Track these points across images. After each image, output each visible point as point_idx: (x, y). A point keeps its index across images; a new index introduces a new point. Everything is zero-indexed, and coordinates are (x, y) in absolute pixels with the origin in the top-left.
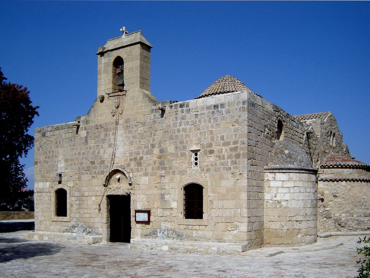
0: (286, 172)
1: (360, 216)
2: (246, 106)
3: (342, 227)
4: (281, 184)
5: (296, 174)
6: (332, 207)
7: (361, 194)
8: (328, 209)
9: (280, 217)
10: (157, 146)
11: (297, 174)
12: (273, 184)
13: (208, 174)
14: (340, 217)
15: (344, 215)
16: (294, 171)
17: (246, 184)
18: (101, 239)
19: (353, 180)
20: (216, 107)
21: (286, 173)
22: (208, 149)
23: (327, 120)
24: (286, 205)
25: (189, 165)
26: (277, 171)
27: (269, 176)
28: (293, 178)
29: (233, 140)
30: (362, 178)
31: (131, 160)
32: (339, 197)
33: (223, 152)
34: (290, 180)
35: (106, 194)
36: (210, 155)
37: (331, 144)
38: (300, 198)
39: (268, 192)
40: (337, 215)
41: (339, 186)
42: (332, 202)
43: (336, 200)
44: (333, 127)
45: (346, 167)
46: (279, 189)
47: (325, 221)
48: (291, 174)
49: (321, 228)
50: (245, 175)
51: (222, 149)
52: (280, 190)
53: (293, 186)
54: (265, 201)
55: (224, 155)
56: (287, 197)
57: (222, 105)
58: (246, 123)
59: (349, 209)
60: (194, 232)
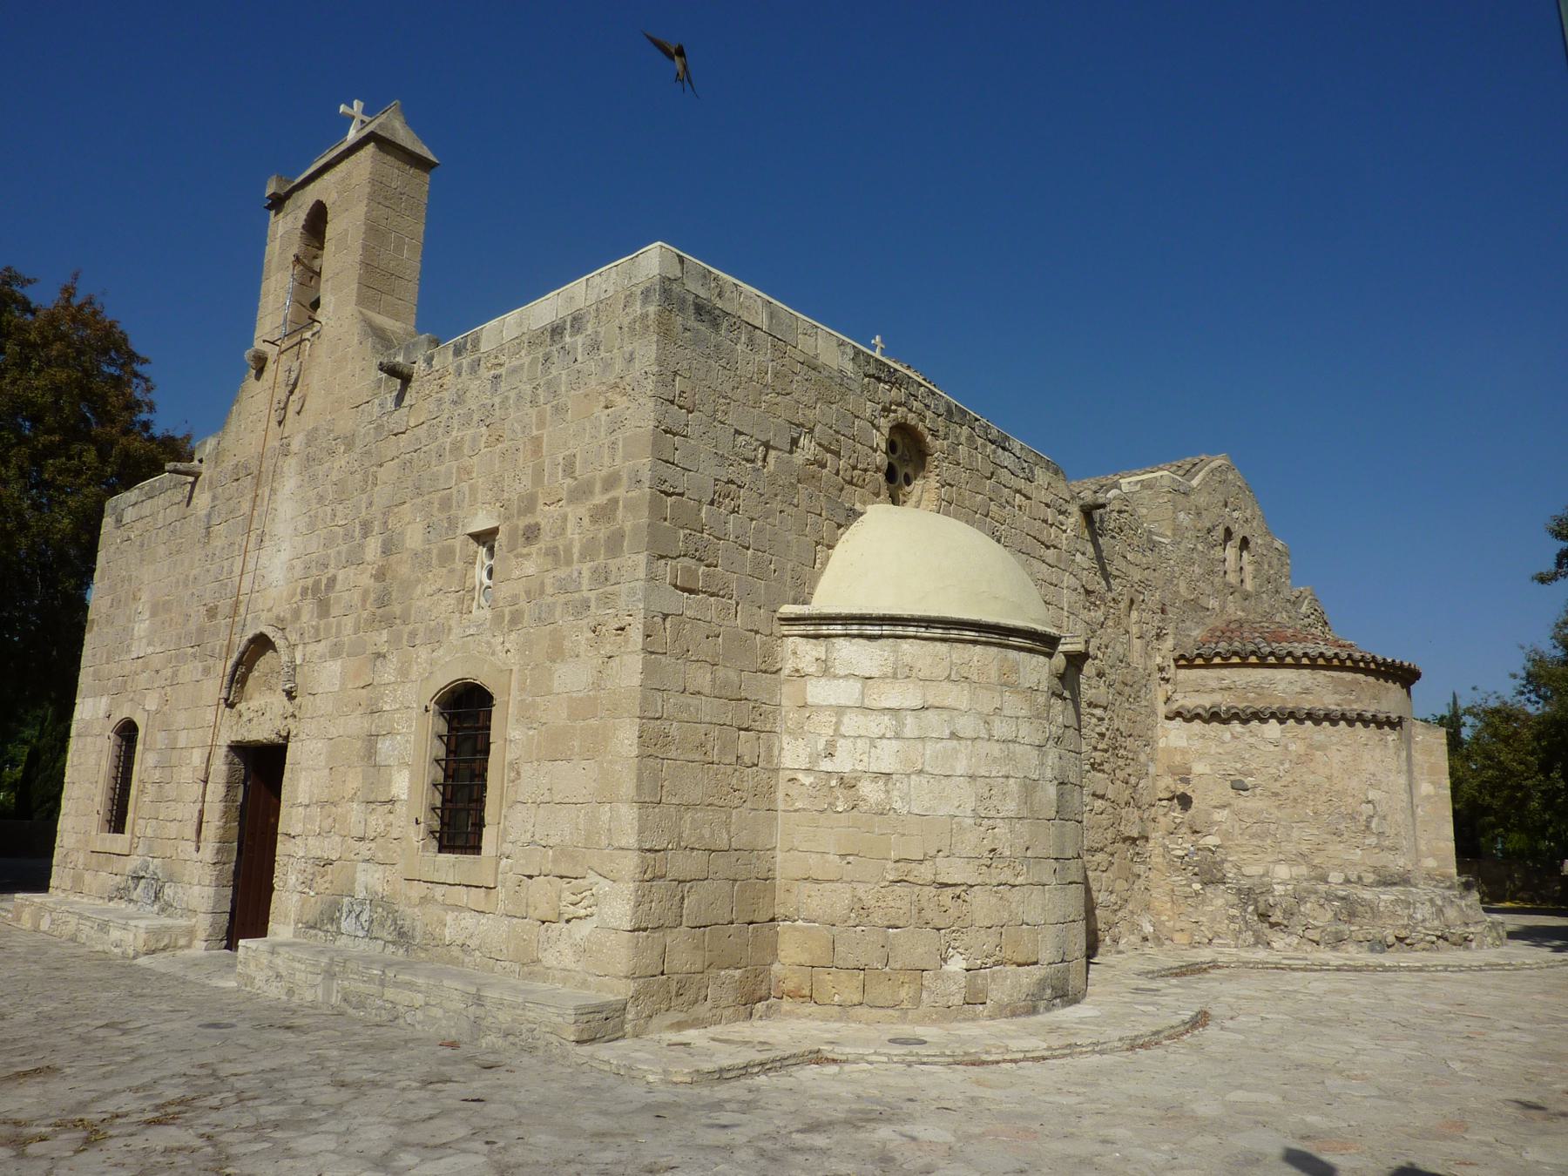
0: (881, 637)
1: (1360, 878)
2: (652, 309)
3: (1272, 925)
4: (857, 695)
5: (930, 644)
6: (1227, 835)
7: (1354, 783)
8: (1211, 841)
9: (850, 858)
10: (377, 527)
11: (938, 644)
12: (819, 692)
13: (513, 636)
14: (1266, 879)
15: (1282, 871)
16: (922, 632)
17: (636, 680)
18: (191, 933)
19: (1314, 717)
20: (556, 331)
21: (880, 642)
22: (522, 523)
23: (1204, 483)
24: (883, 796)
25: (461, 601)
26: (838, 629)
27: (800, 652)
28: (919, 665)
29: (604, 473)
30: (1370, 709)
31: (304, 591)
32: (1258, 791)
33: (569, 531)
34: (900, 673)
35: (226, 738)
36: (525, 551)
37: (1232, 578)
38: (953, 768)
39: (798, 733)
40: (1254, 870)
41: (1252, 740)
42: (1226, 812)
43: (1246, 802)
44: (1236, 514)
45: (1281, 664)
46: (846, 720)
47: (1197, 894)
48: (905, 645)
49: (1179, 925)
50: (636, 635)
51: (565, 518)
52: (851, 723)
53: (918, 703)
54: (784, 776)
55: (572, 541)
56: (887, 757)
57: (577, 321)
58: (650, 385)
59: (1304, 848)
60: (449, 917)
